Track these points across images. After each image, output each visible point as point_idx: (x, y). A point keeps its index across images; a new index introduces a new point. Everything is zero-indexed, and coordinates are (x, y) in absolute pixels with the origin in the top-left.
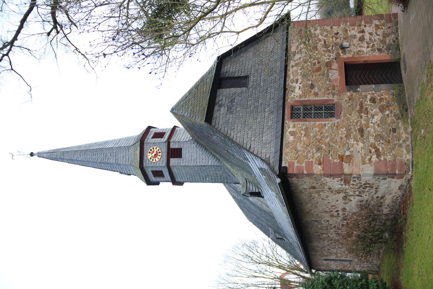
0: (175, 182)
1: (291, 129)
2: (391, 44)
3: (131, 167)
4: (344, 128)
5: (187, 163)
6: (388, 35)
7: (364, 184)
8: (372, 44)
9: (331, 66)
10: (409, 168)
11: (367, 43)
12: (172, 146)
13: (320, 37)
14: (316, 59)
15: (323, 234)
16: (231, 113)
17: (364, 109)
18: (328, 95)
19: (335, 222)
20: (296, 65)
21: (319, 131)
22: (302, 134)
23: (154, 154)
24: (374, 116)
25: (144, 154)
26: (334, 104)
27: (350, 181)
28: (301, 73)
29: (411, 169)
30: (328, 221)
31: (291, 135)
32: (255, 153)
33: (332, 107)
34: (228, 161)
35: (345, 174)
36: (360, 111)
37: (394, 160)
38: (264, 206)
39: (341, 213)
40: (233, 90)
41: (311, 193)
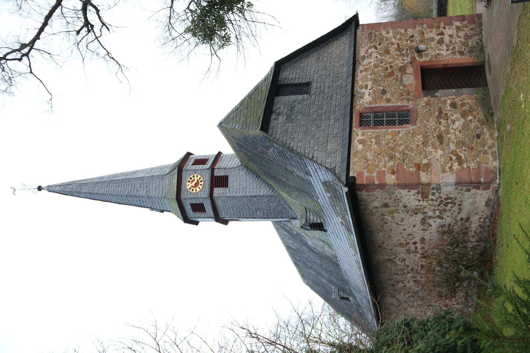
0: (218, 219)
1: (360, 137)
2: (474, 47)
3: (166, 200)
4: (421, 136)
5: (234, 193)
6: (470, 37)
7: (446, 199)
8: (452, 46)
9: (405, 70)
10: (496, 176)
11: (447, 46)
12: (217, 173)
13: (393, 40)
14: (389, 63)
15: (398, 282)
16: (291, 121)
17: (443, 115)
18: (402, 100)
19: (412, 262)
20: (366, 70)
21: (391, 139)
22: (372, 142)
23: (194, 183)
24: (454, 121)
25: (182, 184)
26: (409, 111)
27: (429, 194)
28: (371, 78)
29: (498, 177)
30: (404, 260)
31: (360, 144)
32: (319, 162)
33: (407, 114)
34: (284, 185)
35: (423, 183)
36: (439, 117)
37: (479, 168)
38: (327, 248)
39: (419, 246)
40: (293, 97)
41: (383, 215)
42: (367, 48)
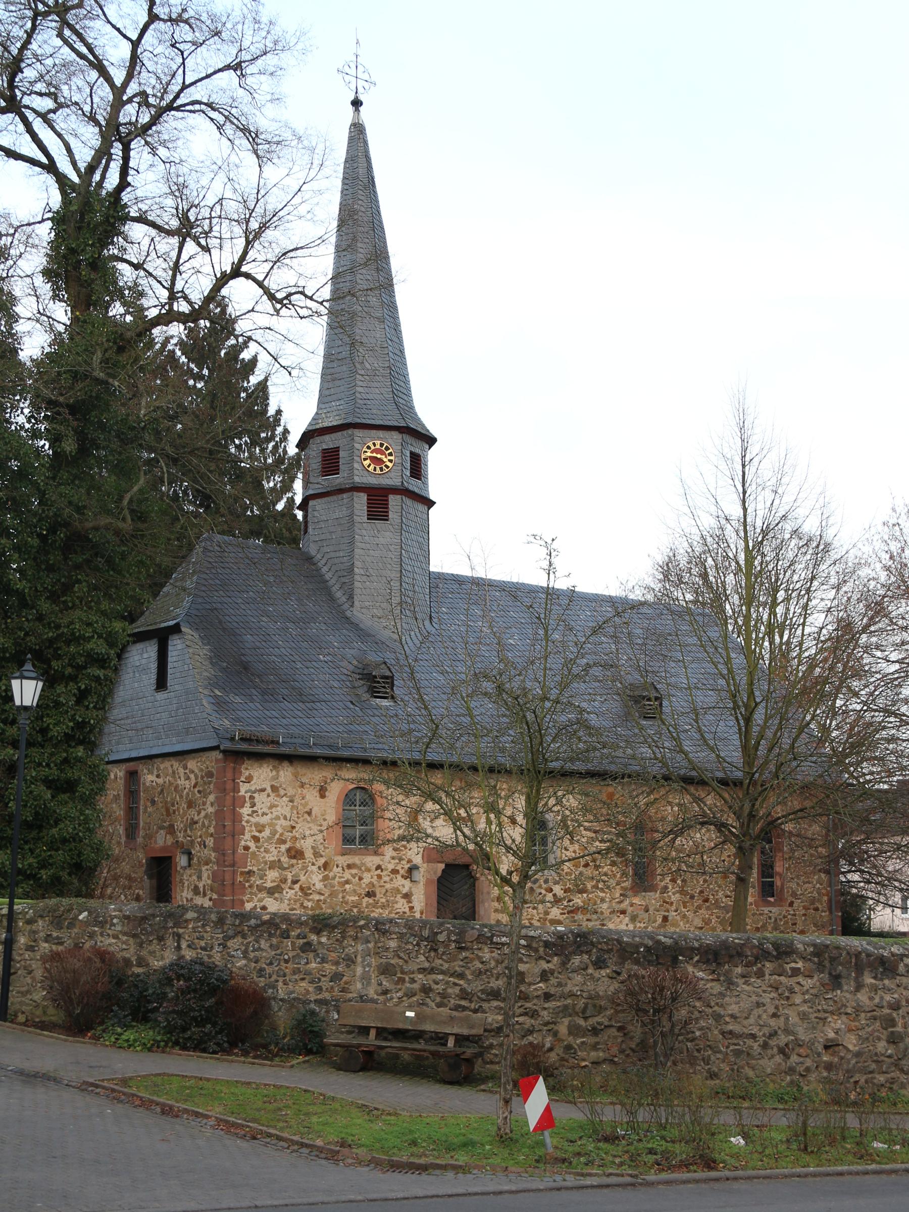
12: (394, 501)
13: (203, 814)
42: (196, 771)
